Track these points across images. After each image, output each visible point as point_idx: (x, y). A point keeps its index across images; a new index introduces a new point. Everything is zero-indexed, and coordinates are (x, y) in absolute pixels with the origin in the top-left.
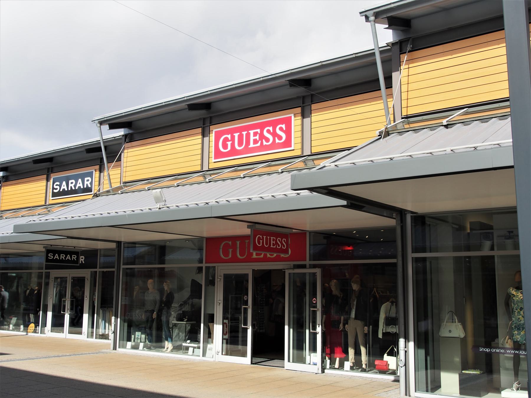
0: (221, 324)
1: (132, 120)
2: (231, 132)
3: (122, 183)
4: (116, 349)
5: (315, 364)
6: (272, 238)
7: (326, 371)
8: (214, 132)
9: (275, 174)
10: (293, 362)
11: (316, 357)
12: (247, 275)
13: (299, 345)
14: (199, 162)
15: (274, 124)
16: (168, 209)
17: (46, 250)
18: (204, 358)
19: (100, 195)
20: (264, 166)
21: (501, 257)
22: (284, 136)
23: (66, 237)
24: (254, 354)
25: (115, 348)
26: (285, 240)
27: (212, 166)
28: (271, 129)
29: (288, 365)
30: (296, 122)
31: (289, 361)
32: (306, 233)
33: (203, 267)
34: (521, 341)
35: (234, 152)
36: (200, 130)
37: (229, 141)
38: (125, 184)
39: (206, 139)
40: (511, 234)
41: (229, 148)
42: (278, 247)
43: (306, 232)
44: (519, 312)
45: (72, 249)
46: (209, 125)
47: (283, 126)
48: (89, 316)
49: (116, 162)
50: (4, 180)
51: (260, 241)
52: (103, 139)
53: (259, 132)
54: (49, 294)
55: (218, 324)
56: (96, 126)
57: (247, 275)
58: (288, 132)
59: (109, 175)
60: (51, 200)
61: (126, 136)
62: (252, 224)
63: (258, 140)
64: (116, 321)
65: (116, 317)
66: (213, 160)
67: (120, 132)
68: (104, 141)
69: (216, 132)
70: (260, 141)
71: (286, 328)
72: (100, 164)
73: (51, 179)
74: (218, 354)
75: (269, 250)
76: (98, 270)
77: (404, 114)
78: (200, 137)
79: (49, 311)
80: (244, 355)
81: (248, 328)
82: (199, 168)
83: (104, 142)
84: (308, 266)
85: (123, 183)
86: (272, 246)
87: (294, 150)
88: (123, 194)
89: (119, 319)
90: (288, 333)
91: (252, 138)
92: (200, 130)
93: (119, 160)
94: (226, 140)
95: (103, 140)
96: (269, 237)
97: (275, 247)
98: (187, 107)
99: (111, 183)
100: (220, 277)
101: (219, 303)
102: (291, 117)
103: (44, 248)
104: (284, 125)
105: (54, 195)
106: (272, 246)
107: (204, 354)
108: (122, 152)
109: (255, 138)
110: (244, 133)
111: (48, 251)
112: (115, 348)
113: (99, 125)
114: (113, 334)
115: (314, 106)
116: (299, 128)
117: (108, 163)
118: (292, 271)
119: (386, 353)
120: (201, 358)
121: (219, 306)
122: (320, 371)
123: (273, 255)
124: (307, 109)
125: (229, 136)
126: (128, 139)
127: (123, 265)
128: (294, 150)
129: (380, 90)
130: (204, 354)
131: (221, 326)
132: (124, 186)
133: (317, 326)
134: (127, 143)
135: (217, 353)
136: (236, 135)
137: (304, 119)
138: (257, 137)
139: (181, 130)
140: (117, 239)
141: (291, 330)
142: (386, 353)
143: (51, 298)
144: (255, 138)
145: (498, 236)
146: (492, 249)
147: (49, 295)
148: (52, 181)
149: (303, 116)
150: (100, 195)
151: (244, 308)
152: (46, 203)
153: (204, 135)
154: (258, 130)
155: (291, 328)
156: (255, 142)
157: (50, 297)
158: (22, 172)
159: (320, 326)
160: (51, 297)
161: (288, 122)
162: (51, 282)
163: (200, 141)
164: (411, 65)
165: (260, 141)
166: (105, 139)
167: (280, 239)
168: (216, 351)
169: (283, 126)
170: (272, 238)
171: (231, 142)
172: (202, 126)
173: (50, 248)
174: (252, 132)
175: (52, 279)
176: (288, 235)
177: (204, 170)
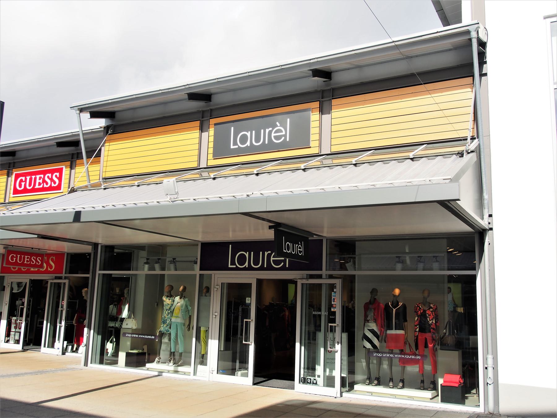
0: (216, 339)
1: (116, 109)
2: (25, 175)
3: (101, 178)
4: (87, 366)
5: (58, 349)
6: (26, 257)
7: (66, 353)
8: (14, 174)
9: (289, 171)
10: (48, 347)
11: (59, 344)
12: (249, 285)
13: (311, 367)
14: (196, 158)
15: (52, 172)
16: (221, 199)
17: (6, 252)
18: (195, 377)
19: (78, 190)
20: (274, 165)
21: (168, 275)
22: (57, 181)
23: (36, 236)
24: (257, 374)
25: (86, 364)
26: (40, 258)
27: (12, 200)
28: (50, 175)
29: (44, 350)
30: (315, 116)
31: (45, 346)
32: (65, 253)
33: (196, 274)
34: (163, 331)
35: (25, 191)
36: (198, 123)
37: (23, 182)
38: (105, 180)
39: (205, 135)
40: (175, 260)
41: (23, 187)
42: (32, 263)
43: (64, 253)
44: (165, 312)
45: (37, 251)
46: (209, 118)
47: (58, 174)
48: (51, 326)
49: (94, 157)
50: (112, 131)
51: (14, 259)
52: (83, 130)
53: (42, 177)
54: (4, 300)
55: (213, 339)
56: (75, 112)
57: (249, 285)
58: (60, 179)
59: (88, 172)
60: (12, 197)
61: (107, 128)
62: (276, 226)
63: (41, 183)
64: (89, 333)
65: (90, 328)
66: (12, 195)
67: (101, 123)
68: (83, 132)
69: (16, 174)
70: (42, 184)
71: (298, 345)
72: (71, 160)
73: (13, 175)
74: (212, 373)
75: (23, 264)
76: (197, 271)
77: (104, 176)
78: (6, 177)
79: (3, 320)
80: (246, 375)
81: (250, 344)
82: (195, 165)
83: (83, 134)
84: (324, 276)
85: (103, 179)
86: (25, 262)
87: (62, 192)
88: (107, 190)
89: (92, 331)
90: (300, 351)
91: (38, 181)
92: (198, 123)
93: (99, 155)
94: (21, 181)
95: (82, 131)
96: (23, 256)
97: (29, 263)
98: (186, 96)
99: (90, 180)
100: (217, 287)
101: (216, 315)
102: (62, 168)
103: (4, 249)
104: (58, 173)
105: (16, 192)
106: (25, 262)
107: (195, 373)
108: (103, 145)
109: (40, 181)
110: (33, 177)
111: (9, 252)
112: (86, 364)
113: (78, 112)
114: (85, 347)
115: (334, 102)
116: (68, 177)
117: (87, 158)
118: (305, 281)
119: (110, 341)
120: (192, 377)
121: (215, 318)
122: (339, 395)
123: (16, 268)
124: (326, 104)
125: (24, 178)
126: (112, 131)
127: (100, 270)
128: (62, 192)
129: (83, 159)
130: (195, 373)
131: (217, 342)
132: (103, 182)
133: (63, 321)
134: (109, 135)
135: (212, 372)
136: (28, 178)
137: (322, 116)
138: (41, 181)
139: (169, 124)
140: (94, 240)
141: (303, 348)
142: (110, 341)
143: (8, 287)
144: (40, 181)
145: (169, 261)
146: (163, 269)
147: (4, 302)
148: (13, 176)
149: (71, 168)
150: (78, 190)
151: (245, 321)
152: (5, 201)
153: (202, 130)
154: (42, 176)
155: (303, 346)
156: (40, 184)
157: (5, 304)
158: (122, 123)
159: (64, 321)
160: (6, 304)
161: (60, 171)
162: (7, 287)
163: (5, 180)
164: (111, 144)
165: (42, 184)
166: (84, 131)
167: (35, 258)
168: (211, 370)
169: (58, 174)
170: (26, 257)
171: (24, 183)
172: (201, 119)
173: (10, 248)
174: (38, 177)
175: (9, 284)
176: (44, 255)
177: (200, 167)
